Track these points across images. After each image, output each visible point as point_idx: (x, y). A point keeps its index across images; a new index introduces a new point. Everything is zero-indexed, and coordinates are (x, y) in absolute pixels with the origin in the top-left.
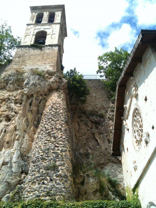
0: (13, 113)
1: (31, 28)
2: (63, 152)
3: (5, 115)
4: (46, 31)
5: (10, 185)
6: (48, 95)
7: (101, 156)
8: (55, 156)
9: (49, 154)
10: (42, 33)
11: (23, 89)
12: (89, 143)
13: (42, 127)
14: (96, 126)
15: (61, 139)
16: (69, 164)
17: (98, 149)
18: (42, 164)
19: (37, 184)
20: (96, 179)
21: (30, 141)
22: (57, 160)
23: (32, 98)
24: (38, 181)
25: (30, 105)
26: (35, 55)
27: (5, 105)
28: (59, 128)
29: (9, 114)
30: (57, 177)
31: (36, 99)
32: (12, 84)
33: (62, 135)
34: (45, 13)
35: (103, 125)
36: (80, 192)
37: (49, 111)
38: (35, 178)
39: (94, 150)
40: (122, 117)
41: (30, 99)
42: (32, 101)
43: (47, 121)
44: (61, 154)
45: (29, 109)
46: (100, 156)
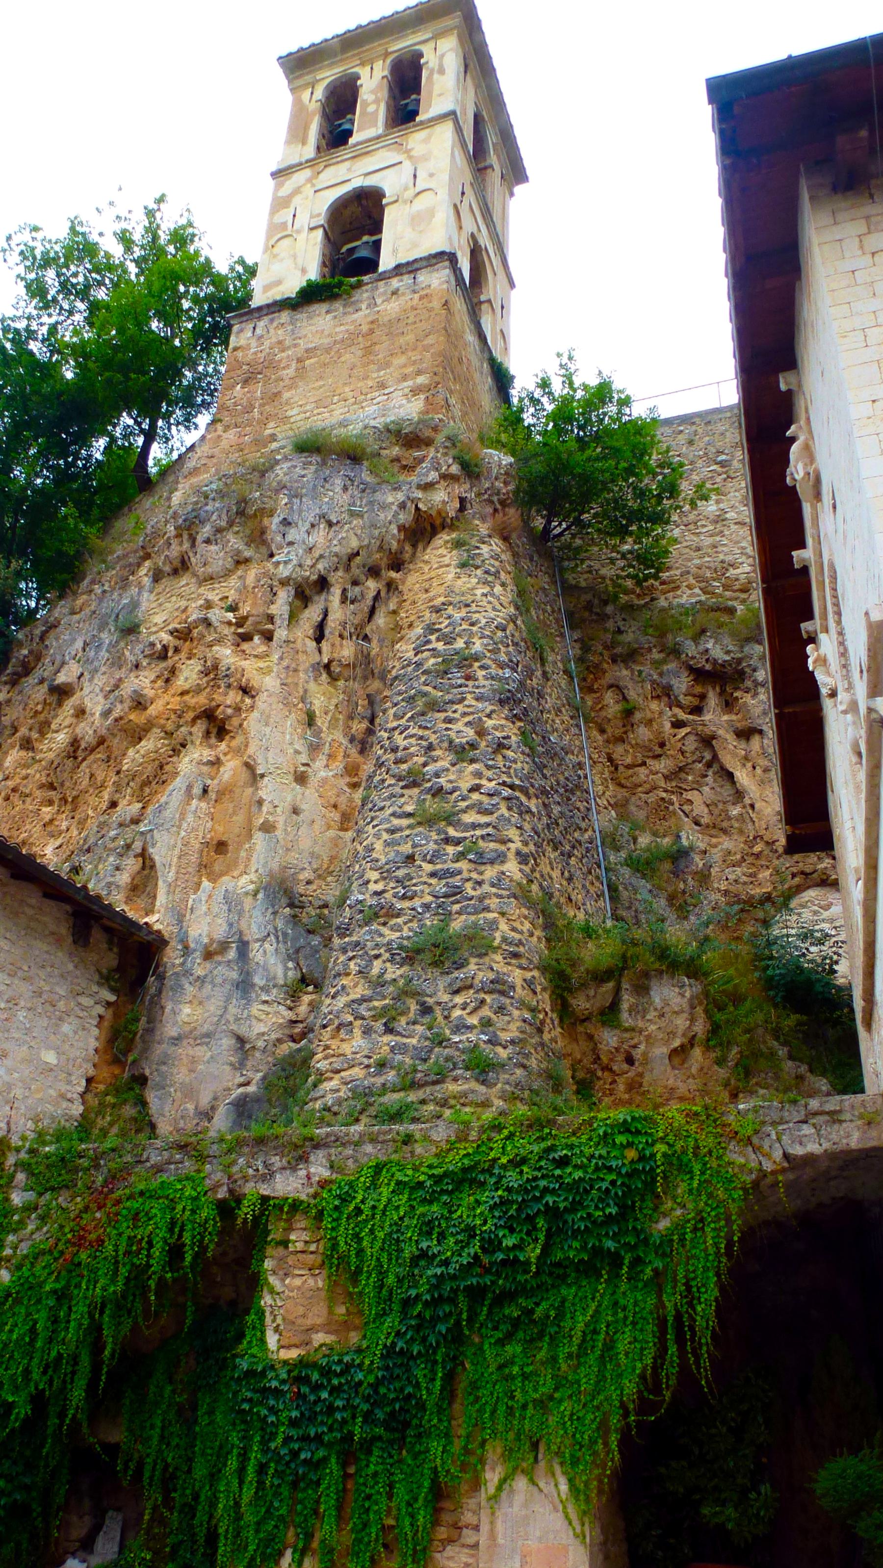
0: (233, 697)
1: (297, 191)
2: (483, 868)
3: (199, 711)
4: (380, 185)
5: (248, 1046)
6: (411, 566)
7: (758, 856)
8: (444, 890)
9: (414, 885)
10: (360, 204)
11: (272, 555)
12: (688, 795)
13: (382, 747)
14: (722, 693)
15: (475, 796)
16: (522, 923)
17: (737, 820)
18: (381, 935)
19: (357, 1032)
20: (681, 987)
21: (329, 827)
22: (456, 907)
23: (326, 600)
24: (363, 1018)
25: (319, 636)
26: (328, 350)
27: (192, 662)
28: (464, 740)
29: (214, 704)
30: (457, 992)
31: (344, 600)
32: (212, 538)
33: (478, 774)
34: (364, 73)
35: (760, 679)
36: (599, 1058)
37: (416, 655)
38: (348, 1005)
39: (713, 832)
40: (803, 626)
41: (315, 606)
42: (326, 614)
43: (405, 714)
44: (474, 875)
45: (317, 658)
46: (750, 860)
